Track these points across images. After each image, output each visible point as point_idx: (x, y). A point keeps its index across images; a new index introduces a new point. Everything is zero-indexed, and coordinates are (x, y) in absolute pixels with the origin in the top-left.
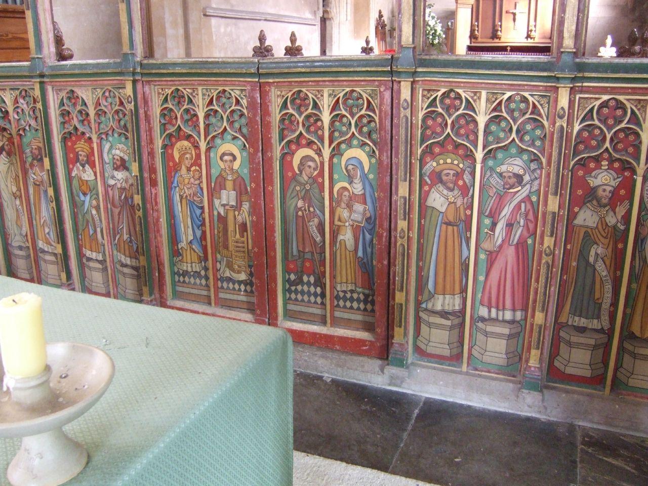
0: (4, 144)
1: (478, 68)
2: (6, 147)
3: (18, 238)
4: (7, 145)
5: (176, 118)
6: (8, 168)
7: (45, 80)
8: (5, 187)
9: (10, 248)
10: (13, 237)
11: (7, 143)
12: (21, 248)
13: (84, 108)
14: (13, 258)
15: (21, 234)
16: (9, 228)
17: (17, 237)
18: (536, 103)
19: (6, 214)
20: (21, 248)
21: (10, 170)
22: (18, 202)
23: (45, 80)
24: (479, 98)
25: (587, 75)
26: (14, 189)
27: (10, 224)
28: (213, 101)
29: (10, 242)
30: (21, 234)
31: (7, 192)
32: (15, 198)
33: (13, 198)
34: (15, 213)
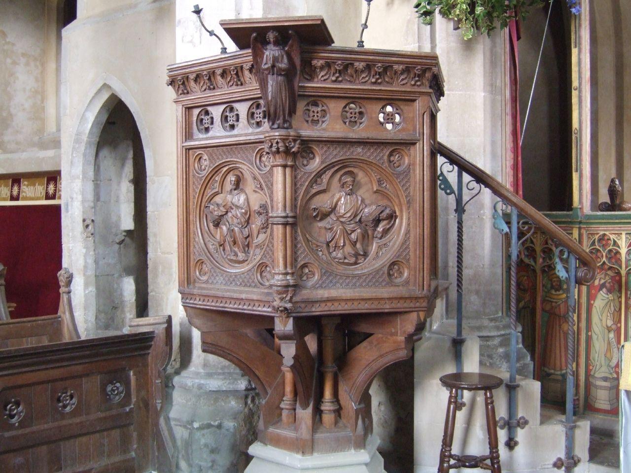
0: (606, 282)
1: (610, 215)
2: (607, 285)
3: (604, 369)
4: (609, 283)
5: (602, 256)
6: (606, 305)
7: (582, 226)
8: (599, 321)
9: (591, 380)
10: (598, 367)
11: (610, 280)
12: (605, 379)
13: (531, 245)
14: (593, 389)
15: (609, 366)
16: (594, 360)
17: (603, 369)
18: (616, 239)
19: (593, 346)
20: (605, 379)
21: (608, 305)
22: (612, 335)
23: (582, 226)
24: (621, 238)
25: (591, 221)
26: (610, 323)
27: (597, 355)
28: (595, 242)
29: (592, 373)
30: (609, 366)
31: (599, 325)
32: (609, 332)
33: (606, 331)
34: (606, 345)
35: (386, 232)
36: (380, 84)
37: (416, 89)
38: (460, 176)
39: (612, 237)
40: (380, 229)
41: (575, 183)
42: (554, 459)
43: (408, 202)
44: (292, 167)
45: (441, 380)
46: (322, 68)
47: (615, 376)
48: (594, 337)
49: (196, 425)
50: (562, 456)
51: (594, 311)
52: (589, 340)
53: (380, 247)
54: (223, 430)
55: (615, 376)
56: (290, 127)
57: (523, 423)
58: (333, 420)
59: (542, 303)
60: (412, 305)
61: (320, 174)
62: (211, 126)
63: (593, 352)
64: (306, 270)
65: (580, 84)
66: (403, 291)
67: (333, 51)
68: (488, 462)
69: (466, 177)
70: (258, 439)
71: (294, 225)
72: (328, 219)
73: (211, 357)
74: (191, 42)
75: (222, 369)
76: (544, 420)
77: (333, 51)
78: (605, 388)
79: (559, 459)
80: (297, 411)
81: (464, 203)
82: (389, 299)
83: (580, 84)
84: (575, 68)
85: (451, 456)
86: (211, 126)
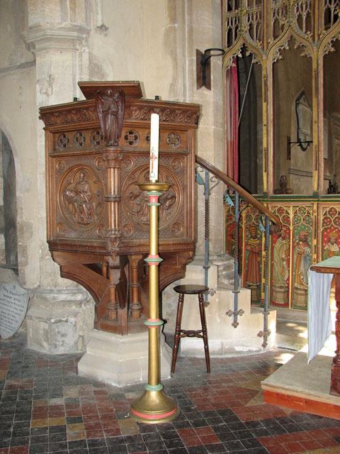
12: (281, 287)
20: (281, 287)
22: (284, 263)
26: (284, 256)
35: (170, 206)
36: (167, 121)
37: (187, 124)
38: (207, 174)
39: (285, 208)
40: (167, 204)
41: (265, 178)
42: (258, 332)
43: (183, 189)
44: (118, 168)
45: (174, 289)
46: (136, 110)
47: (287, 285)
48: (275, 264)
49: (53, 321)
50: (262, 330)
51: (275, 249)
52: (272, 265)
53: (167, 215)
54: (69, 323)
55: (287, 285)
56: (118, 145)
57: (241, 312)
58: (138, 315)
59: (246, 246)
60: (185, 247)
61: (134, 172)
62: (134, 141)
63: (274, 274)
64: (126, 229)
65: (267, 123)
66: (179, 240)
67: (141, 102)
68: (201, 334)
69: (211, 175)
70: (332, 359)
71: (119, 202)
72: (138, 199)
73: (66, 281)
74: (46, 93)
75: (66, 287)
76: (253, 311)
77: (141, 102)
78: (281, 292)
79: (261, 332)
80: (118, 310)
81: (210, 187)
82: (173, 244)
83: (267, 123)
84: (264, 114)
85: (181, 331)
86: (134, 141)
